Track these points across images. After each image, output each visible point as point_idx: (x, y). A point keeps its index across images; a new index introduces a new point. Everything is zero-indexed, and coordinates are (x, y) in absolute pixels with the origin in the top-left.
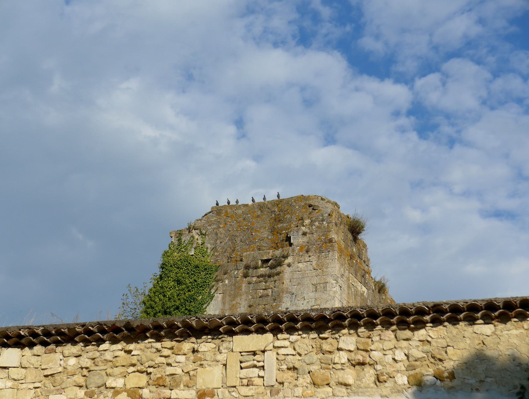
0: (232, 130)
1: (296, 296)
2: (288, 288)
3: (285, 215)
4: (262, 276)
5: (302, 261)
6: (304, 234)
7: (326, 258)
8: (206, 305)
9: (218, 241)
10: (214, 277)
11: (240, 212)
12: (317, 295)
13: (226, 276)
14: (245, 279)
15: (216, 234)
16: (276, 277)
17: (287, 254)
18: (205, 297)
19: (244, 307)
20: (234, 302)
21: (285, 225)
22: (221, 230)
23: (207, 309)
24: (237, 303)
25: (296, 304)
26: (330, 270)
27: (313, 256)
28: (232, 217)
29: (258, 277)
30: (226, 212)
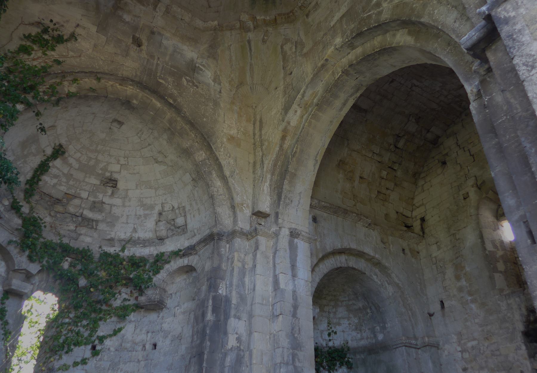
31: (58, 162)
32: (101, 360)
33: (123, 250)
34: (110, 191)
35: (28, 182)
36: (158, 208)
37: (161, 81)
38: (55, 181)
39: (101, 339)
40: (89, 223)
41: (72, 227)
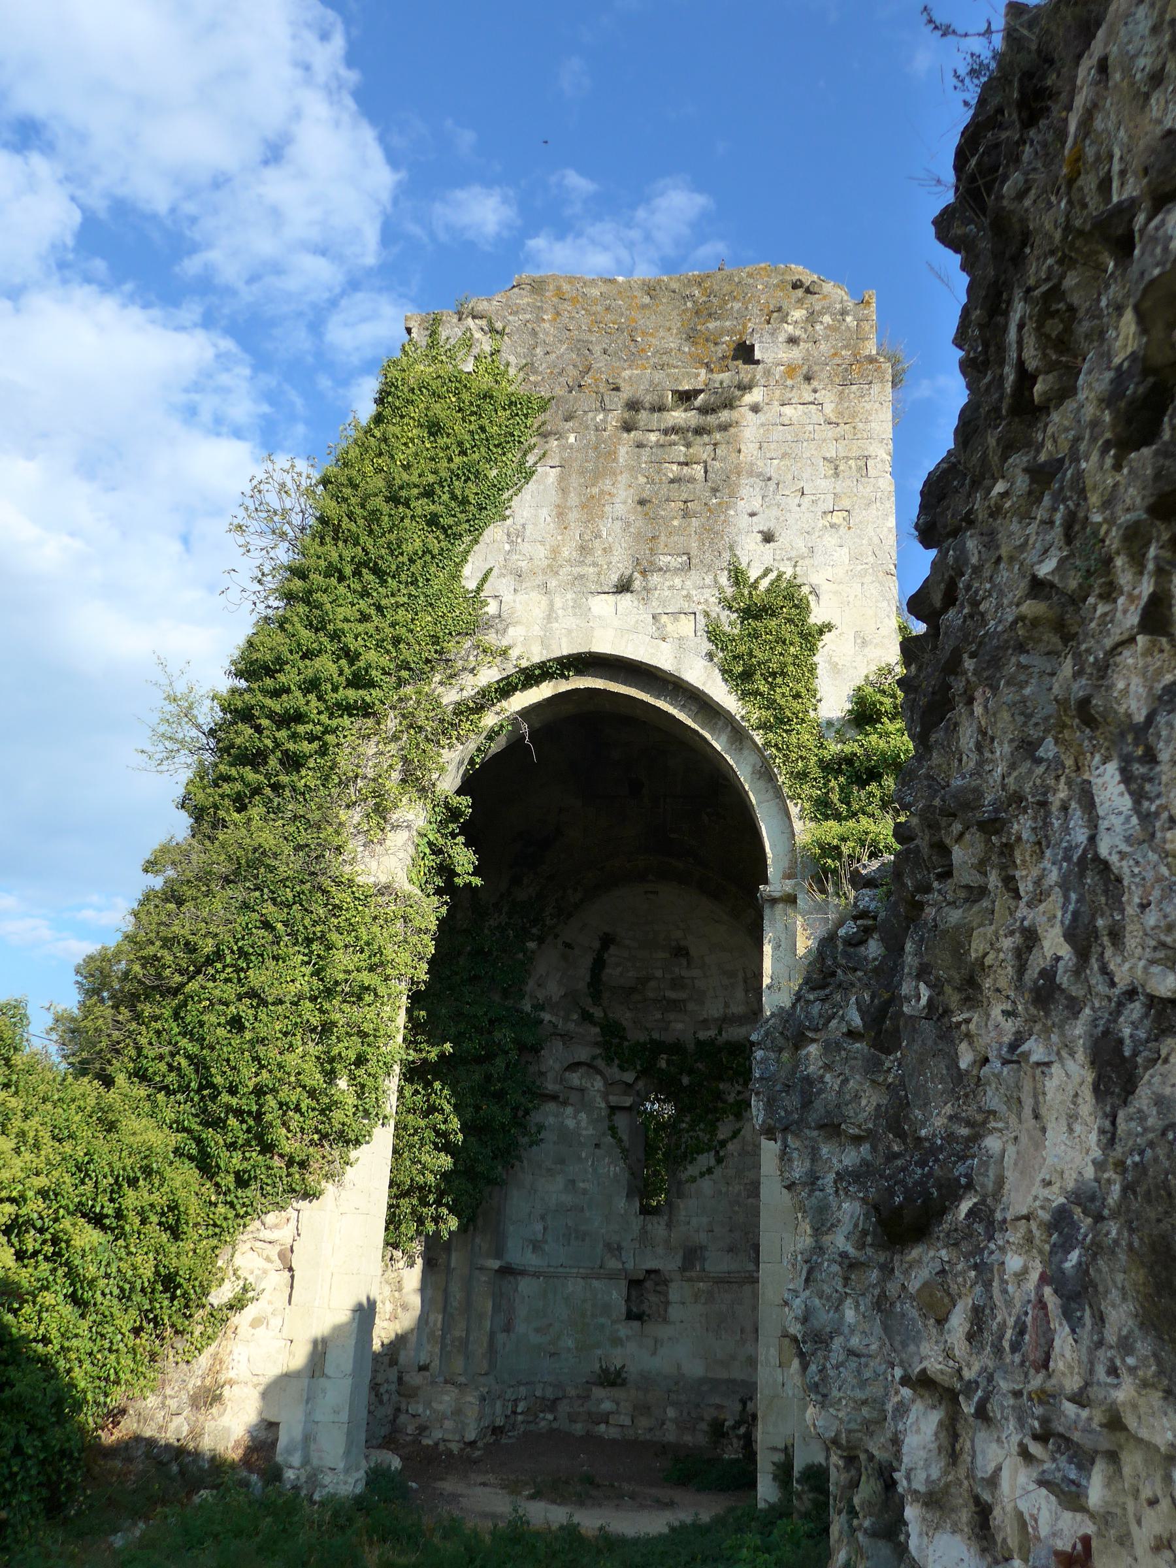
0: (176, 547)
1: (778, 484)
2: (752, 464)
3: (725, 302)
4: (674, 430)
5: (793, 401)
6: (792, 341)
7: (862, 397)
8: (511, 492)
9: (538, 350)
10: (536, 425)
11: (595, 292)
12: (840, 486)
13: (571, 424)
14: (625, 435)
15: (534, 333)
16: (718, 436)
17: (752, 380)
18: (509, 472)
19: (625, 503)
20: (595, 490)
21: (728, 323)
22: (547, 325)
23: (512, 503)
24: (602, 492)
25: (779, 505)
26: (878, 428)
27: (823, 392)
28: (574, 300)
29: (666, 432)
30: (559, 288)
31: (613, 950)
32: (726, 1167)
33: (720, 1033)
34: (684, 962)
35: (590, 985)
36: (741, 975)
37: (672, 836)
38: (619, 969)
39: (723, 1144)
40: (676, 1006)
41: (658, 1016)
